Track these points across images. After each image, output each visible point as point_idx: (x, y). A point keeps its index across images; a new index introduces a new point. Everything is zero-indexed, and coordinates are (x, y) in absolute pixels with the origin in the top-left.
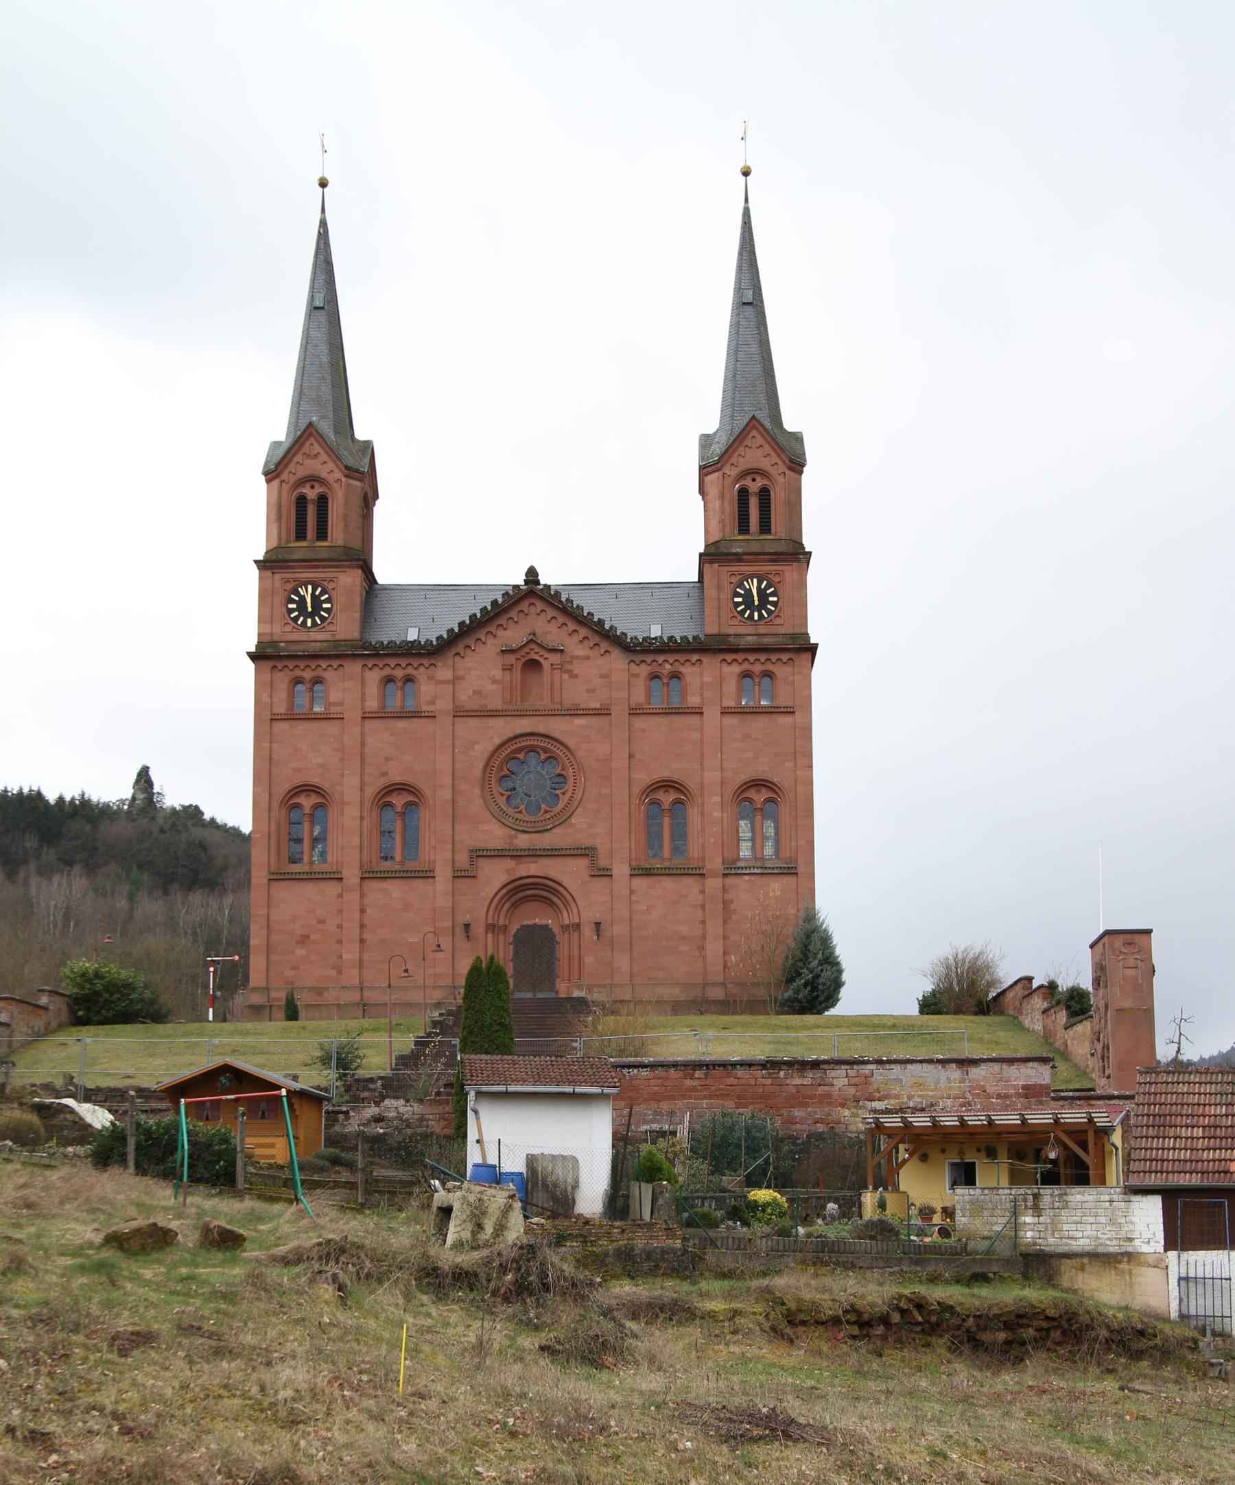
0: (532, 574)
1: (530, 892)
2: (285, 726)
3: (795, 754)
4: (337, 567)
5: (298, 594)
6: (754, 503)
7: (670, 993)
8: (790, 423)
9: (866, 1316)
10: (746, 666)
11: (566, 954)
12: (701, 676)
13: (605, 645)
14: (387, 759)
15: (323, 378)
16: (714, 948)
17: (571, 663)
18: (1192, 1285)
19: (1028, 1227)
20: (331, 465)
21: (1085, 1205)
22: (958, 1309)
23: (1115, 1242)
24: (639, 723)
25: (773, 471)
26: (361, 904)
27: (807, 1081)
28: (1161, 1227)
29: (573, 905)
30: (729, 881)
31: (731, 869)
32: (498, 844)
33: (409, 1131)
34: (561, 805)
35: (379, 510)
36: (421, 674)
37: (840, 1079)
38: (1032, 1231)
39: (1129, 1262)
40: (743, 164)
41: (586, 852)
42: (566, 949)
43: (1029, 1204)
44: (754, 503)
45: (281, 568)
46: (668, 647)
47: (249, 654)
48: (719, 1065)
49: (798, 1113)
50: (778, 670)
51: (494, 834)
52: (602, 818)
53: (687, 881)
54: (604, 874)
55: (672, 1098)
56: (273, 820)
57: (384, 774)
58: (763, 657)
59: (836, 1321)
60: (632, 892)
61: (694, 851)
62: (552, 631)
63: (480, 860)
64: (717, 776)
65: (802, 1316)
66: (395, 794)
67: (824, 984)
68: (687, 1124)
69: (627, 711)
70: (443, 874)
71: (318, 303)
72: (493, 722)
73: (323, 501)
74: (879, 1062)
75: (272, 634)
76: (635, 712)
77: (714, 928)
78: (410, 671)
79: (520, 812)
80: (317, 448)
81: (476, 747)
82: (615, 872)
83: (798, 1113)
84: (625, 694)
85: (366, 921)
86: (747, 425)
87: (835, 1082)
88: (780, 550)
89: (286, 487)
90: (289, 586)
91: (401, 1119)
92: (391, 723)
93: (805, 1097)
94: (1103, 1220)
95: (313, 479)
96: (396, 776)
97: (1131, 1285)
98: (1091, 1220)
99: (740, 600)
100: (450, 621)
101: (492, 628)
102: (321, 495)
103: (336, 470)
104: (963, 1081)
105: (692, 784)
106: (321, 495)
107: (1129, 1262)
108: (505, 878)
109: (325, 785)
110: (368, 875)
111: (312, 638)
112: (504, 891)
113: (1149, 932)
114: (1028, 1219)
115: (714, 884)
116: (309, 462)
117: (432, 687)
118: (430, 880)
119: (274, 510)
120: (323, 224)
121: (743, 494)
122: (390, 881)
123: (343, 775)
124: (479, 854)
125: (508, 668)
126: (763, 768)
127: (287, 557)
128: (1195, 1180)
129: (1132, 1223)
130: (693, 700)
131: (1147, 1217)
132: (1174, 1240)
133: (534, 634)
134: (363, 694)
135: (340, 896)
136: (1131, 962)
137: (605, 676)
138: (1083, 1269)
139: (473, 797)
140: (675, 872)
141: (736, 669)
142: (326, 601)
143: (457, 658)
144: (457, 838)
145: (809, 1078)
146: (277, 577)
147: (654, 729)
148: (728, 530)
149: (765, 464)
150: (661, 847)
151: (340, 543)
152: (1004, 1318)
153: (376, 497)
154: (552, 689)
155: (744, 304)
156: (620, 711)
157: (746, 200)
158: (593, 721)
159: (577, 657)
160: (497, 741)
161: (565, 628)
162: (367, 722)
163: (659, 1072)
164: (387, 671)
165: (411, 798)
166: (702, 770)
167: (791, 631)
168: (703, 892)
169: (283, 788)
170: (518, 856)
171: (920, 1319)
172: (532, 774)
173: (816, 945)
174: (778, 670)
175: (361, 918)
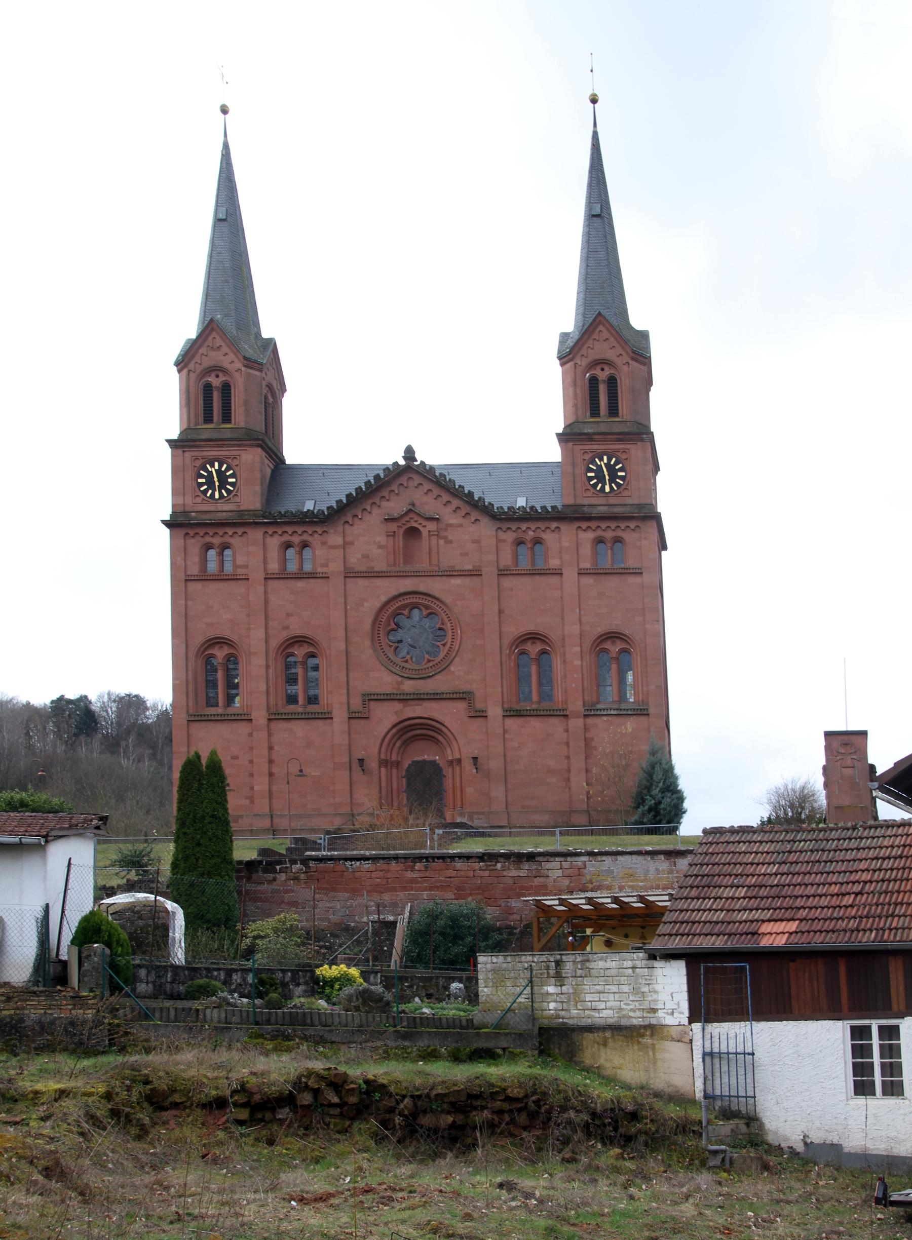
0: (409, 453)
1: (431, 733)
2: (198, 586)
3: (644, 609)
4: (239, 446)
5: (206, 470)
6: (603, 389)
7: (541, 818)
8: (637, 321)
9: (257, 1098)
10: (599, 533)
11: (451, 786)
12: (560, 542)
13: (475, 515)
14: (288, 615)
15: (227, 281)
16: (579, 782)
17: (446, 530)
18: (716, 1061)
19: (551, 998)
20: (231, 357)
21: (608, 973)
22: (392, 1089)
23: (638, 1014)
24: (507, 582)
25: (618, 361)
26: (269, 742)
27: (523, 873)
28: (685, 996)
29: (454, 742)
30: (590, 721)
31: (591, 712)
32: (388, 689)
33: (141, 923)
34: (442, 655)
35: (289, 404)
36: (315, 540)
37: (554, 870)
38: (553, 1002)
39: (652, 1035)
40: (591, 92)
41: (464, 696)
42: (450, 781)
43: (552, 972)
44: (603, 389)
45: (191, 447)
46: (529, 516)
47: (164, 522)
48: (438, 858)
49: (514, 903)
50: (628, 537)
51: (383, 680)
52: (478, 669)
53: (552, 721)
54: (481, 715)
55: (394, 889)
56: (190, 668)
57: (287, 628)
58: (613, 525)
59: (220, 1103)
60: (505, 731)
61: (559, 696)
62: (429, 503)
63: (372, 703)
64: (576, 629)
65: (177, 1098)
66: (296, 646)
67: (665, 809)
68: (407, 914)
69: (496, 572)
70: (340, 715)
71: (221, 216)
72: (378, 582)
73: (226, 389)
74: (591, 854)
75: (184, 505)
76: (503, 573)
77: (578, 762)
78: (306, 537)
79: (406, 661)
80: (219, 342)
81: (366, 604)
82: (490, 713)
83: (514, 903)
84: (493, 557)
85: (274, 757)
86: (594, 320)
87: (550, 873)
88: (626, 430)
89: (193, 375)
90: (198, 463)
91: (133, 911)
92: (291, 583)
93: (522, 888)
94: (626, 989)
95: (217, 369)
96: (296, 630)
97: (655, 1061)
98: (614, 988)
99: (593, 474)
100: (340, 492)
102: (229, 387)
103: (236, 360)
104: (670, 872)
105: (554, 636)
106: (229, 387)
107: (652, 1035)
108: (394, 719)
109: (234, 638)
110: (274, 717)
111: (220, 509)
112: (394, 731)
113: (864, 734)
114: (551, 989)
115: (576, 724)
116: (212, 354)
117: (325, 552)
118: (329, 721)
119: (184, 397)
120: (226, 146)
121: (594, 381)
122: (293, 722)
123: (249, 629)
124: (370, 698)
126: (616, 623)
127: (195, 437)
128: (719, 943)
129: (656, 992)
130: (554, 563)
131: (670, 986)
132: (703, 1008)
133: (413, 505)
134: (265, 558)
135: (250, 735)
136: (849, 762)
137: (476, 542)
138: (605, 1044)
139: (364, 649)
140: (542, 713)
141: (590, 535)
142: (231, 476)
143: (346, 526)
144: (351, 683)
145: (525, 869)
146: (187, 455)
147: (521, 589)
148: (580, 412)
149: (611, 355)
150: (530, 692)
151: (242, 425)
152: (452, 1099)
153: (283, 389)
154: (430, 553)
155: (594, 216)
156: (490, 572)
158: (467, 581)
159: (451, 525)
160: (384, 599)
161: (440, 499)
162: (270, 582)
163: (380, 864)
164: (286, 538)
165: (311, 649)
166: (563, 624)
167: (637, 502)
168: (567, 731)
169: (198, 640)
170: (404, 699)
171: (336, 1100)
172: (415, 626)
173: (658, 775)
174: (628, 537)
175: (270, 755)
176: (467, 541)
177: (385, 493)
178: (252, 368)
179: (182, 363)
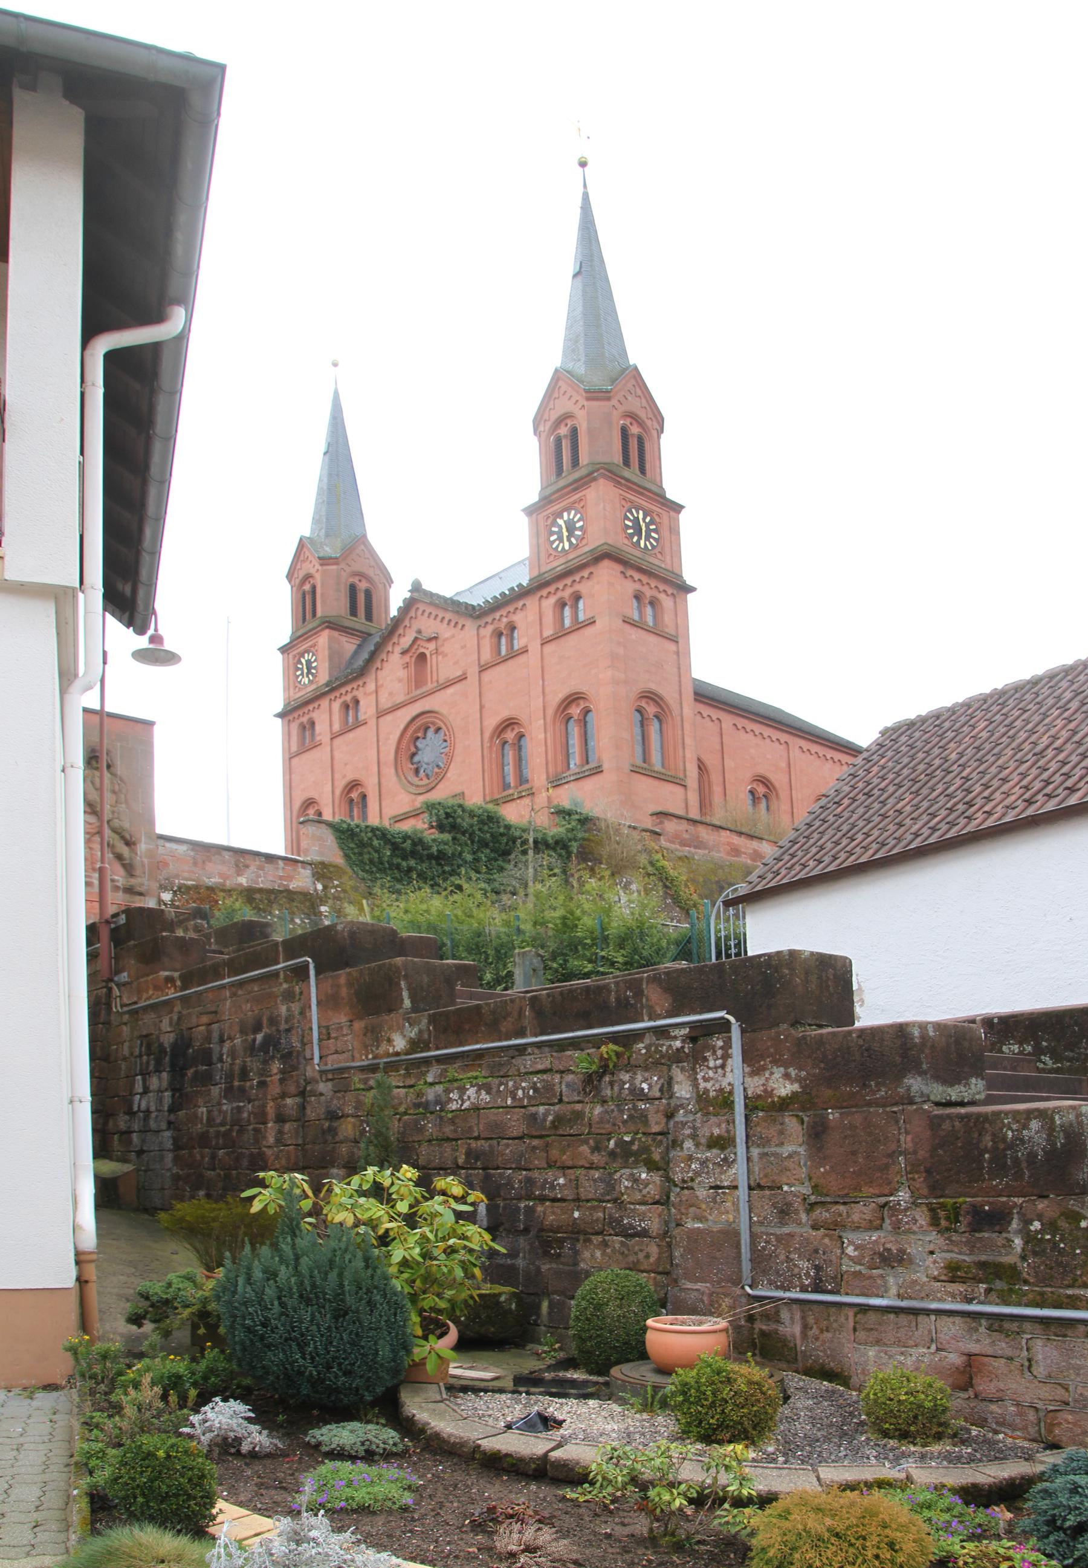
101: (395, 640)
105: (523, 718)
120: (586, 197)
125: (407, 666)
157: (585, 186)
176: (460, 649)
177: (401, 631)
178: (328, 564)
179: (290, 576)
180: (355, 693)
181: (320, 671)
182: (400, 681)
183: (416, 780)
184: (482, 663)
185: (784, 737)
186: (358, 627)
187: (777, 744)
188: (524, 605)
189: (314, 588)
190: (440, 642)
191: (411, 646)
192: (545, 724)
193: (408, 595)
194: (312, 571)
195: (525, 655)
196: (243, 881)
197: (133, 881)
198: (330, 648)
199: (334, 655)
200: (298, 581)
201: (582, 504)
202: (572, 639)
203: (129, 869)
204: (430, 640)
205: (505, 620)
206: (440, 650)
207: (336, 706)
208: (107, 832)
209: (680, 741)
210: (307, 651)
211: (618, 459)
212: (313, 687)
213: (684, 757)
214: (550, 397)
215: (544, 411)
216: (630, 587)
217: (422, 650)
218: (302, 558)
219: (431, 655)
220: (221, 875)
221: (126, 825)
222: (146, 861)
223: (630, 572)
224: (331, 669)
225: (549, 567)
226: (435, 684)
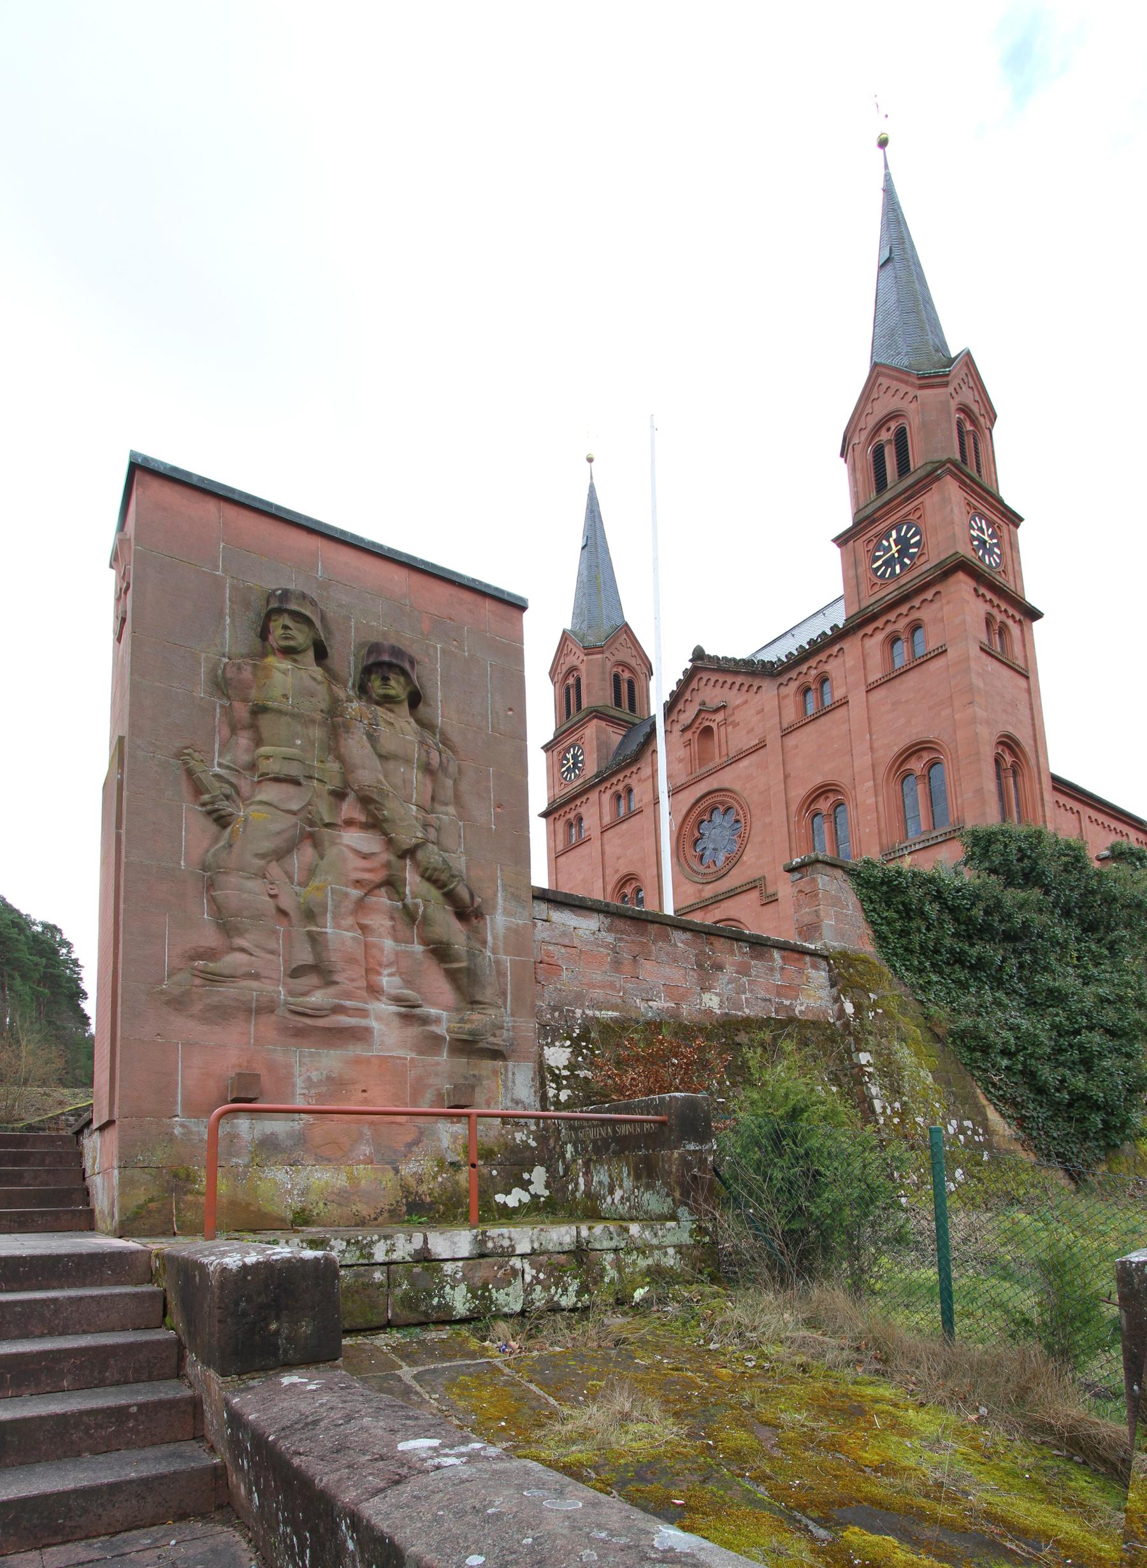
58: (904, 609)
64: (867, 759)
105: (844, 781)
120: (888, 178)
125: (688, 744)
154: (720, 746)
157: (886, 166)
159: (738, 706)
179: (553, 673)
180: (627, 781)
181: (587, 762)
182: (681, 761)
183: (701, 869)
184: (785, 726)
185: (1077, 806)
186: (623, 716)
187: (1070, 813)
188: (842, 649)
189: (578, 681)
190: (729, 711)
191: (694, 720)
192: (875, 785)
193: (689, 665)
194: (577, 663)
195: (843, 710)
196: (712, 1001)
197: (477, 1019)
198: (598, 739)
199: (602, 745)
200: (561, 676)
201: (918, 514)
202: (911, 679)
203: (466, 983)
204: (717, 710)
205: (813, 672)
206: (730, 720)
207: (607, 797)
208: (411, 878)
209: (1039, 797)
210: (573, 746)
211: (958, 456)
212: (581, 781)
213: (1044, 816)
214: (868, 398)
215: (860, 415)
216: (982, 608)
217: (707, 723)
218: (565, 652)
219: (719, 727)
220: (671, 990)
221: (459, 862)
222: (507, 960)
223: (982, 590)
224: (599, 759)
225: (873, 600)
226: (725, 759)
